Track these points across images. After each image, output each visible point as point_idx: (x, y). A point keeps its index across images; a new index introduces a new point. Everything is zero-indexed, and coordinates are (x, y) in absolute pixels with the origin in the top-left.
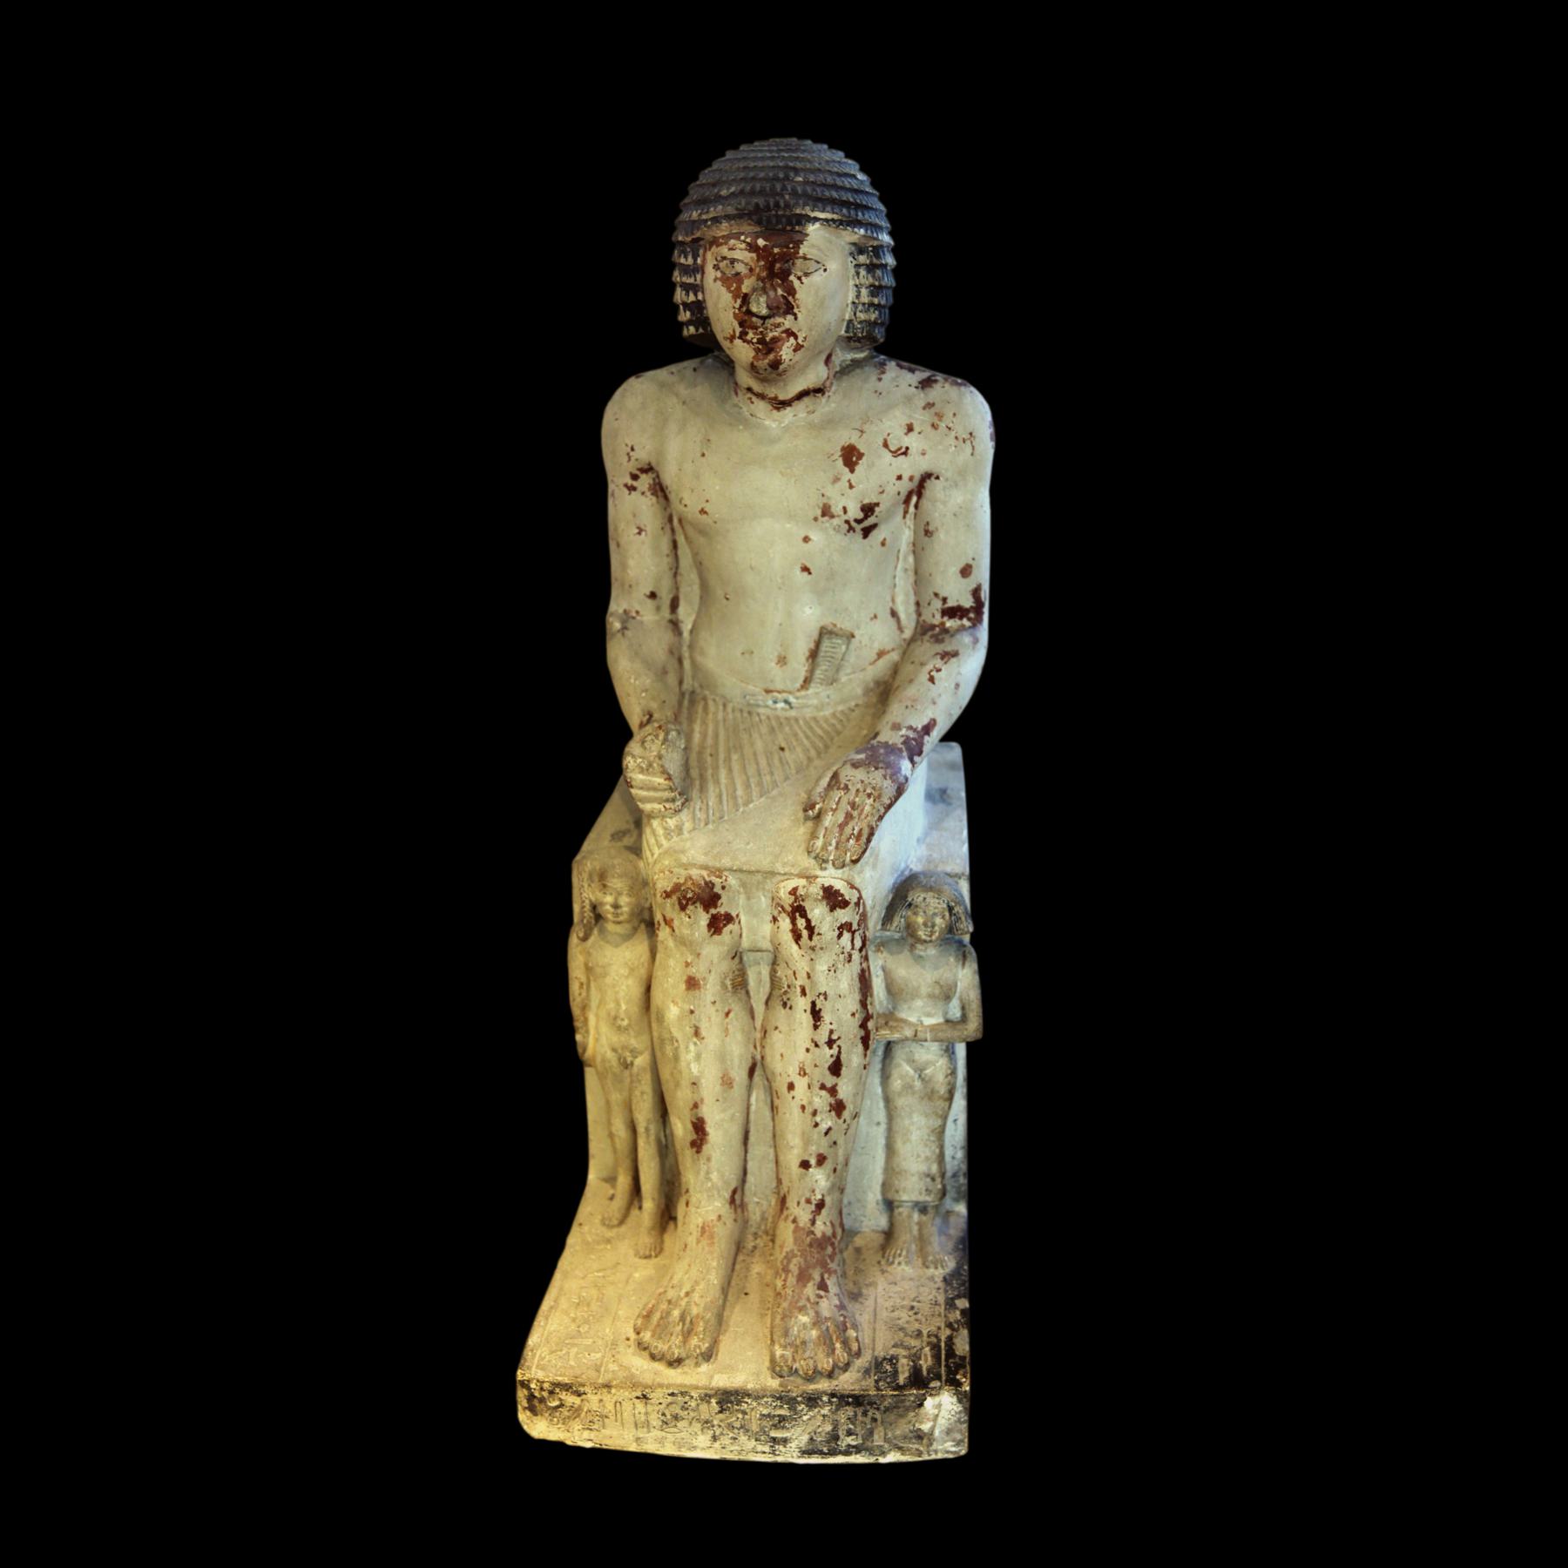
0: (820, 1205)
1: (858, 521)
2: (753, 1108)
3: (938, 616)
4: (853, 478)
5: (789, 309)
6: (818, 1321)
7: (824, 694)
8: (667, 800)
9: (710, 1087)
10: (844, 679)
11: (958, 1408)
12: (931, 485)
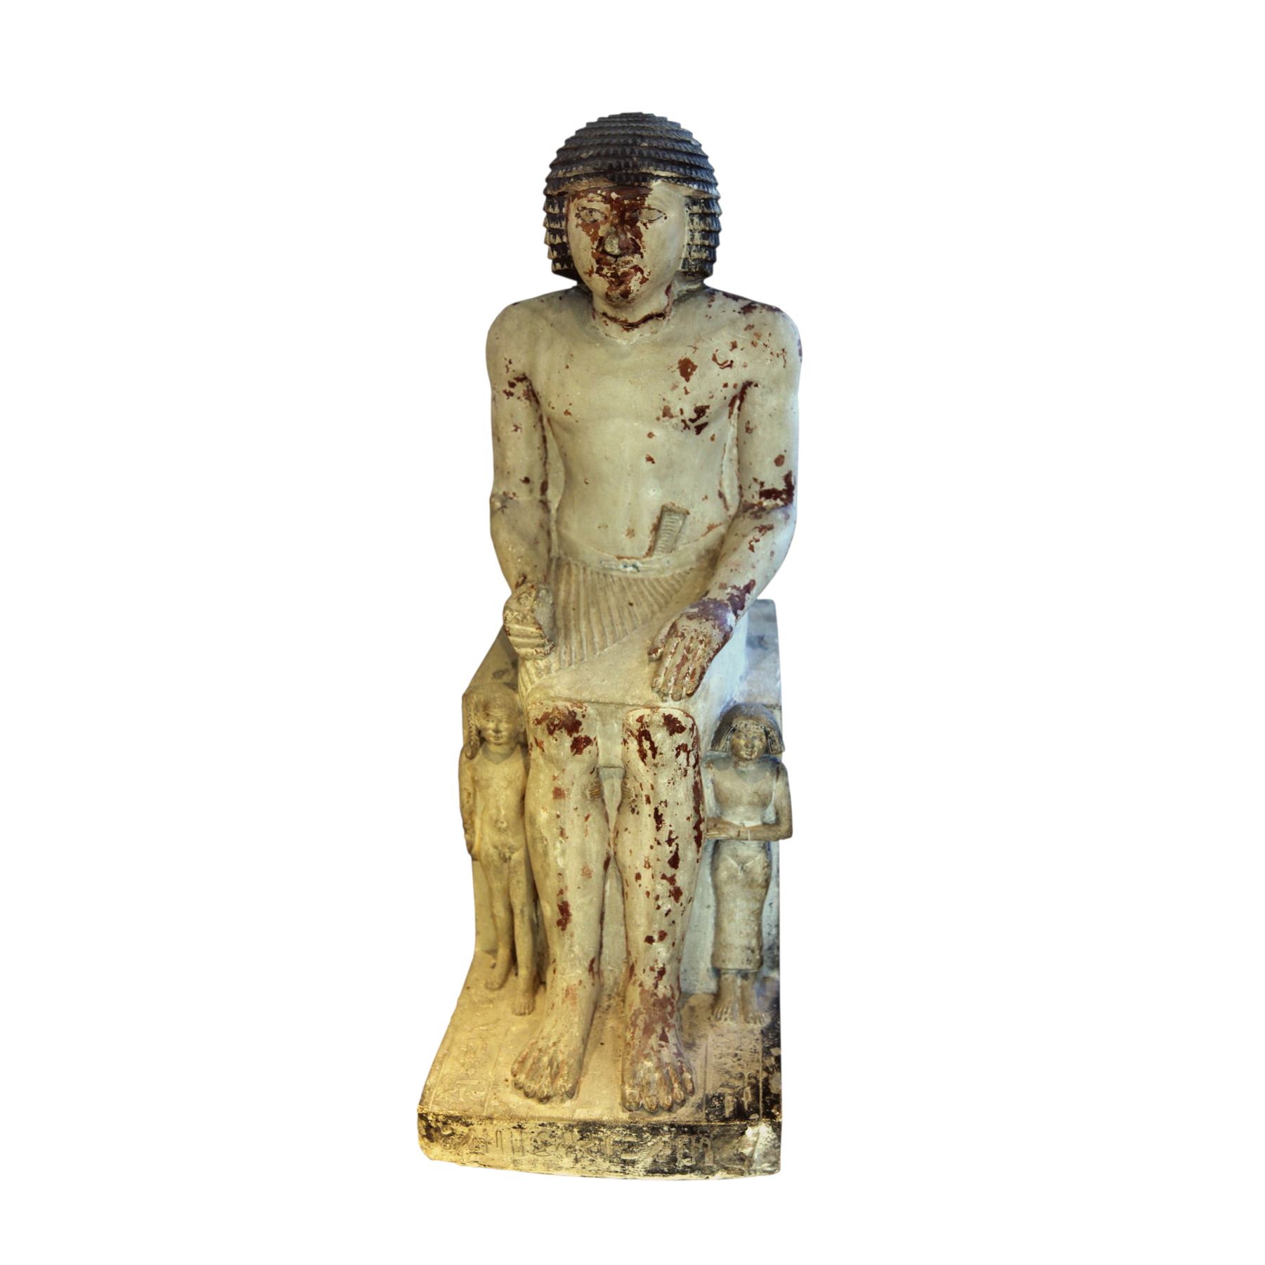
0: (662, 972)
1: (692, 421)
2: (607, 894)
3: (757, 497)
4: (689, 385)
5: (637, 249)
6: (660, 1066)
7: (665, 560)
8: (538, 646)
9: (573, 877)
10: (681, 548)
12: (751, 391)
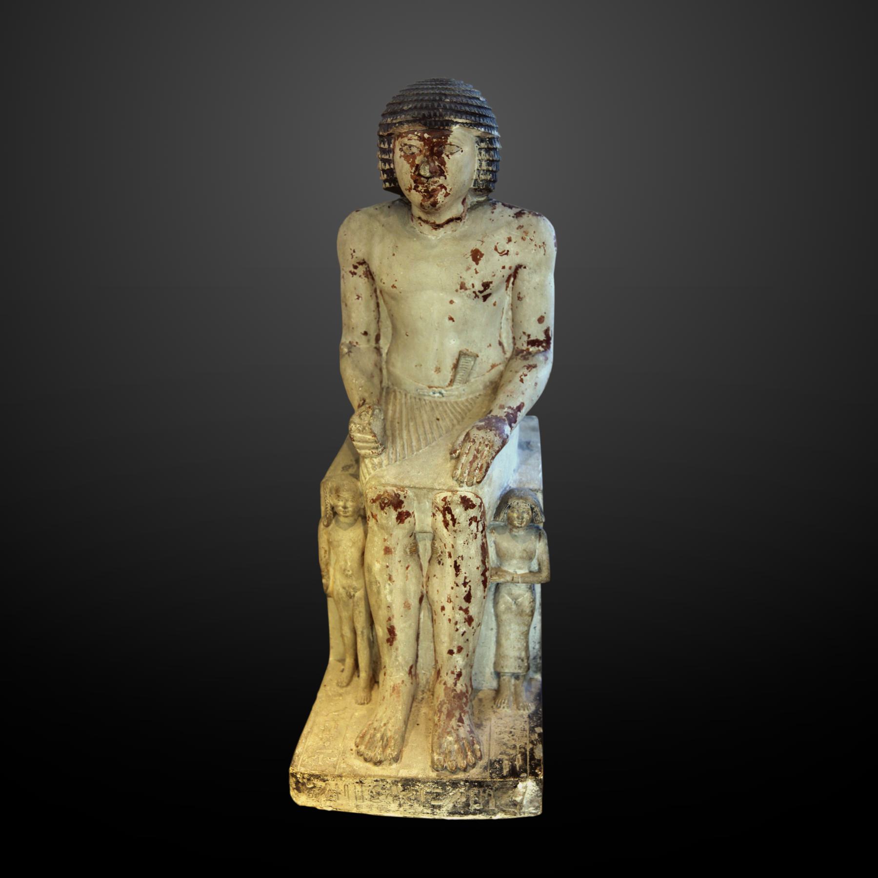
0: (459, 675)
1: (481, 292)
2: (422, 620)
3: (525, 345)
4: (478, 268)
5: (442, 173)
6: (458, 740)
7: (461, 389)
8: (374, 448)
9: (398, 609)
10: (472, 380)
11: (537, 788)
12: (521, 271)
